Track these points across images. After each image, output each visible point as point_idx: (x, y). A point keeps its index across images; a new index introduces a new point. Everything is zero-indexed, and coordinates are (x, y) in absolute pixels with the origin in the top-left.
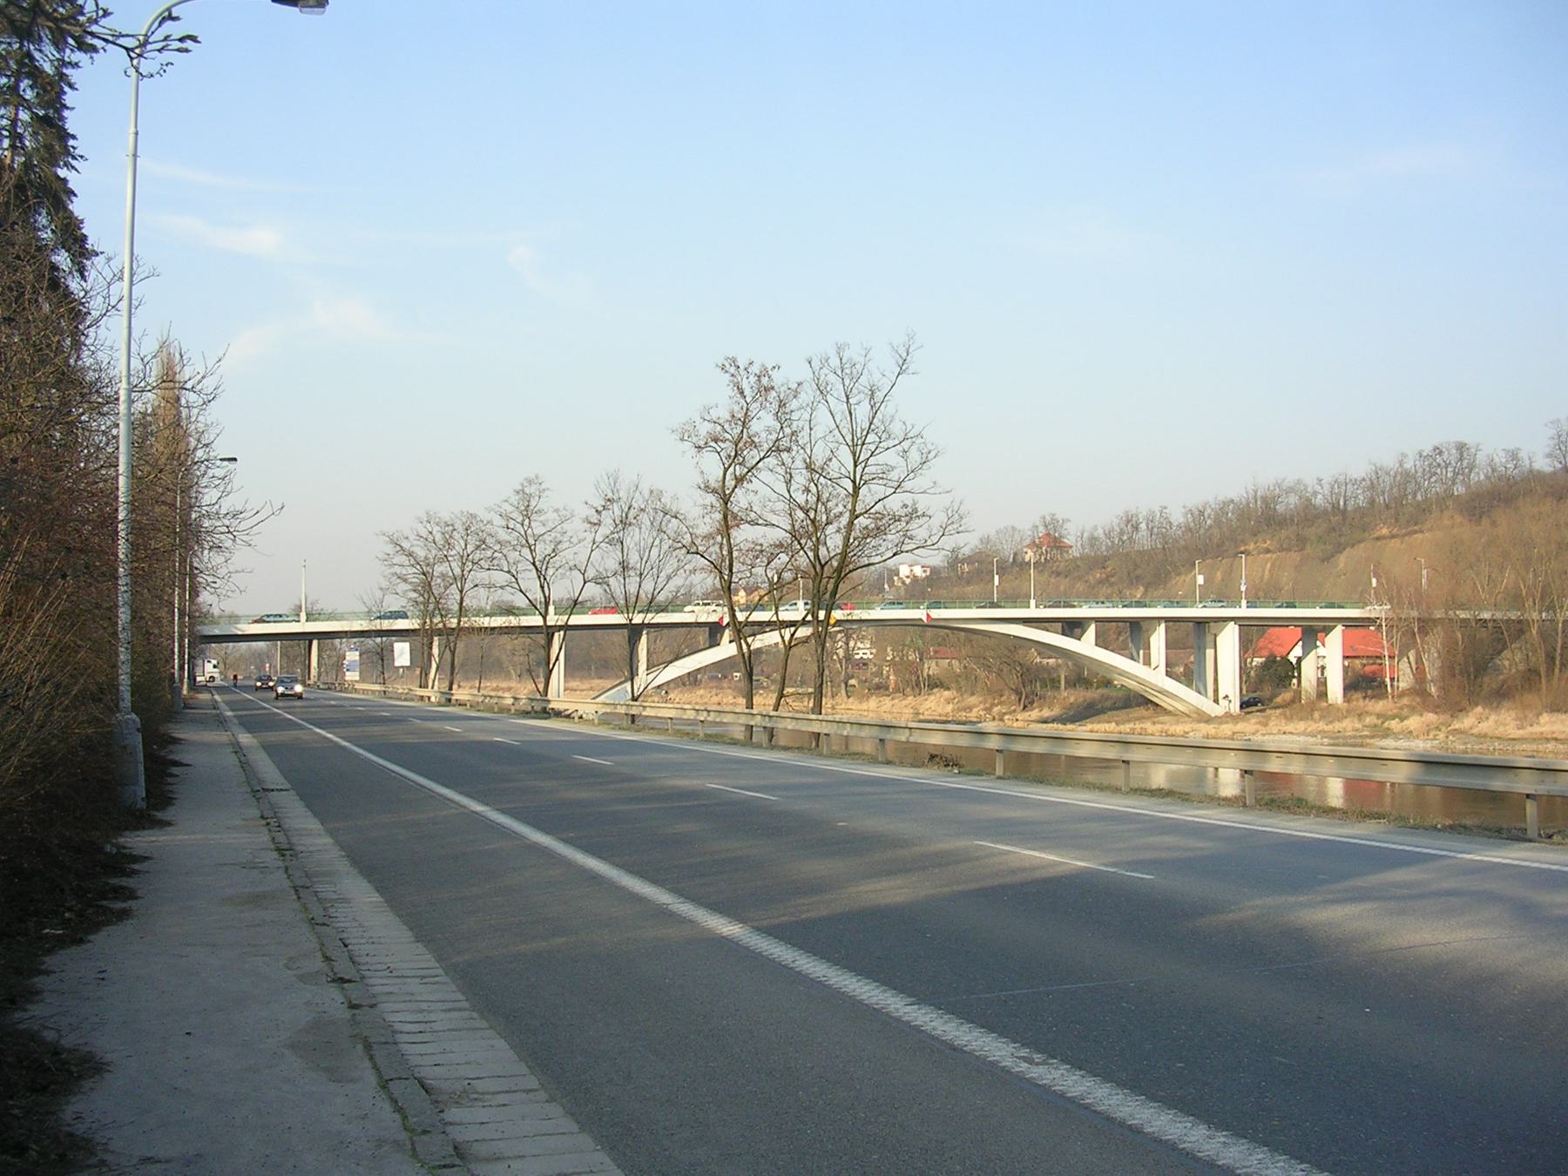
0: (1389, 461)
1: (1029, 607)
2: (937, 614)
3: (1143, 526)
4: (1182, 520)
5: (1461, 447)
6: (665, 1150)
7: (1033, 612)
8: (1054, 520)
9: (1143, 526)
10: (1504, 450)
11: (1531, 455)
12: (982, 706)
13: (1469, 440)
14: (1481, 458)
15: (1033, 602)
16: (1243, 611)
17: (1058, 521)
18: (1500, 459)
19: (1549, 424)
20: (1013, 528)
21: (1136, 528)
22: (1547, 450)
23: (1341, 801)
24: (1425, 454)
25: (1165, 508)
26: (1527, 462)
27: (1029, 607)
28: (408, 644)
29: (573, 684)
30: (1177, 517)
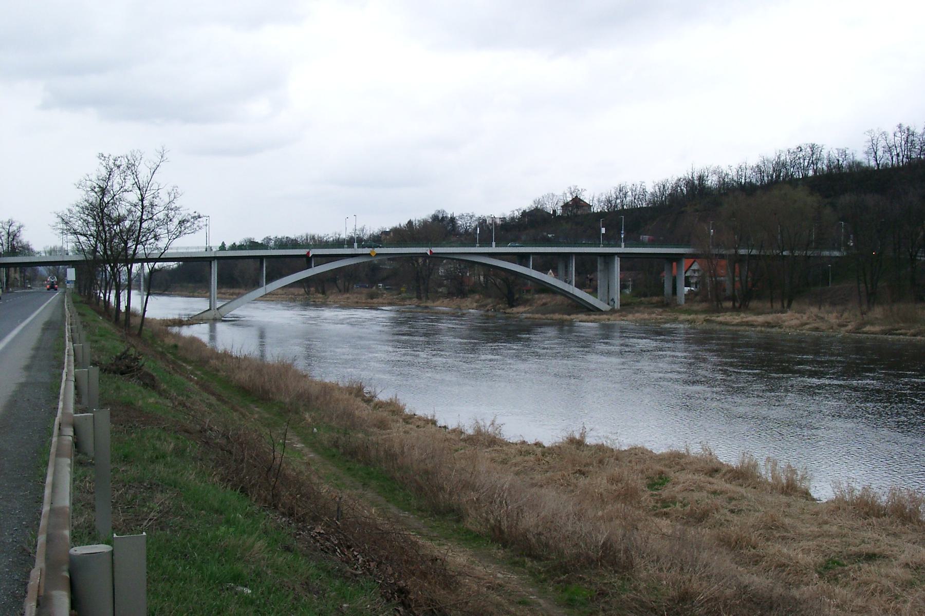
0: (772, 156)
1: (492, 246)
2: (435, 250)
3: (630, 193)
4: (652, 190)
5: (812, 147)
6: (379, 564)
7: (494, 249)
8: (576, 189)
9: (630, 193)
10: (837, 149)
11: (854, 152)
12: (492, 305)
13: (818, 143)
14: (825, 154)
15: (494, 243)
16: (622, 249)
17: (579, 191)
18: (835, 155)
19: (867, 133)
20: (553, 195)
21: (625, 195)
22: (866, 149)
23: (318, 379)
24: (791, 151)
25: (643, 182)
26: (851, 157)
27: (492, 246)
28: (74, 269)
29: (223, 290)
30: (650, 189)
